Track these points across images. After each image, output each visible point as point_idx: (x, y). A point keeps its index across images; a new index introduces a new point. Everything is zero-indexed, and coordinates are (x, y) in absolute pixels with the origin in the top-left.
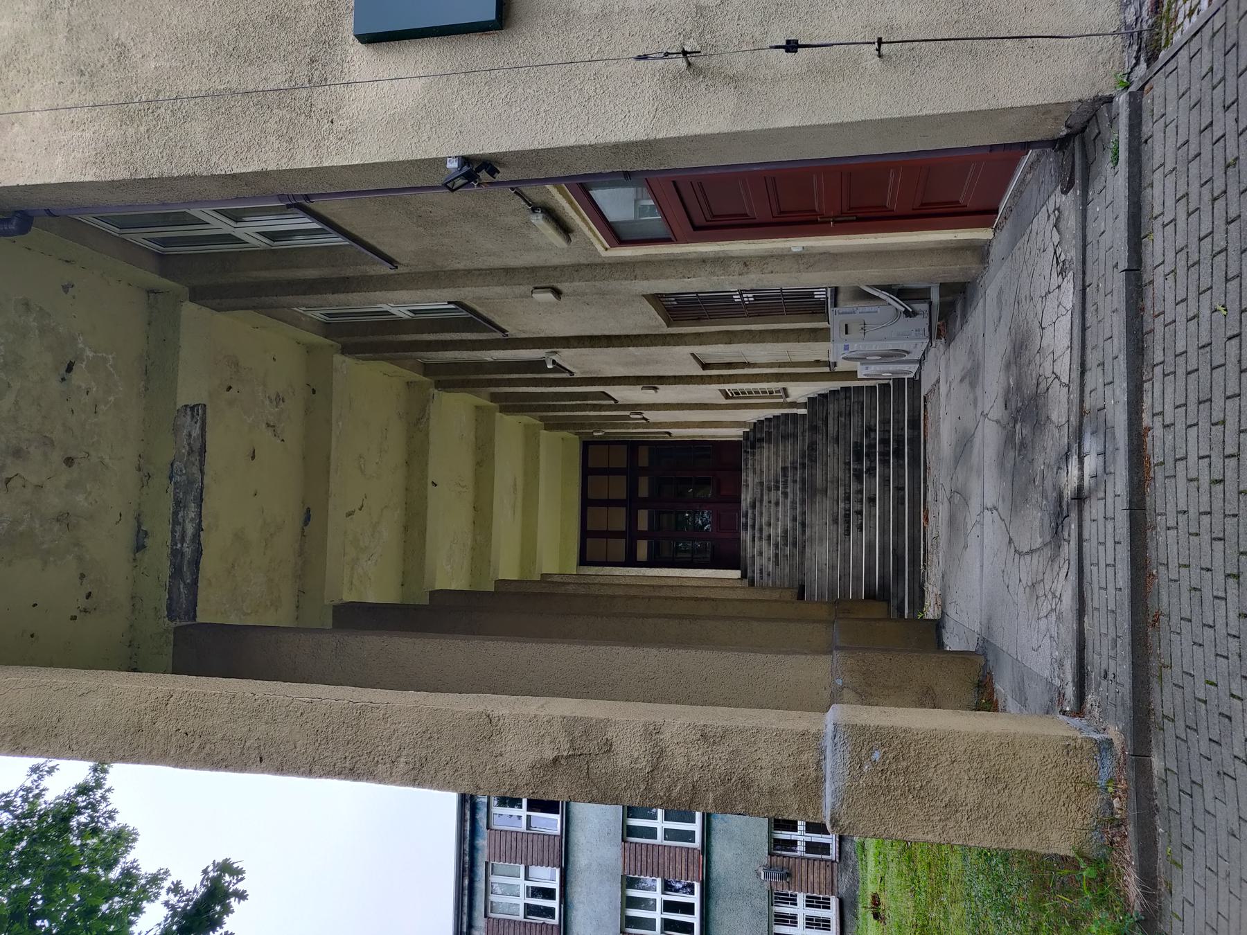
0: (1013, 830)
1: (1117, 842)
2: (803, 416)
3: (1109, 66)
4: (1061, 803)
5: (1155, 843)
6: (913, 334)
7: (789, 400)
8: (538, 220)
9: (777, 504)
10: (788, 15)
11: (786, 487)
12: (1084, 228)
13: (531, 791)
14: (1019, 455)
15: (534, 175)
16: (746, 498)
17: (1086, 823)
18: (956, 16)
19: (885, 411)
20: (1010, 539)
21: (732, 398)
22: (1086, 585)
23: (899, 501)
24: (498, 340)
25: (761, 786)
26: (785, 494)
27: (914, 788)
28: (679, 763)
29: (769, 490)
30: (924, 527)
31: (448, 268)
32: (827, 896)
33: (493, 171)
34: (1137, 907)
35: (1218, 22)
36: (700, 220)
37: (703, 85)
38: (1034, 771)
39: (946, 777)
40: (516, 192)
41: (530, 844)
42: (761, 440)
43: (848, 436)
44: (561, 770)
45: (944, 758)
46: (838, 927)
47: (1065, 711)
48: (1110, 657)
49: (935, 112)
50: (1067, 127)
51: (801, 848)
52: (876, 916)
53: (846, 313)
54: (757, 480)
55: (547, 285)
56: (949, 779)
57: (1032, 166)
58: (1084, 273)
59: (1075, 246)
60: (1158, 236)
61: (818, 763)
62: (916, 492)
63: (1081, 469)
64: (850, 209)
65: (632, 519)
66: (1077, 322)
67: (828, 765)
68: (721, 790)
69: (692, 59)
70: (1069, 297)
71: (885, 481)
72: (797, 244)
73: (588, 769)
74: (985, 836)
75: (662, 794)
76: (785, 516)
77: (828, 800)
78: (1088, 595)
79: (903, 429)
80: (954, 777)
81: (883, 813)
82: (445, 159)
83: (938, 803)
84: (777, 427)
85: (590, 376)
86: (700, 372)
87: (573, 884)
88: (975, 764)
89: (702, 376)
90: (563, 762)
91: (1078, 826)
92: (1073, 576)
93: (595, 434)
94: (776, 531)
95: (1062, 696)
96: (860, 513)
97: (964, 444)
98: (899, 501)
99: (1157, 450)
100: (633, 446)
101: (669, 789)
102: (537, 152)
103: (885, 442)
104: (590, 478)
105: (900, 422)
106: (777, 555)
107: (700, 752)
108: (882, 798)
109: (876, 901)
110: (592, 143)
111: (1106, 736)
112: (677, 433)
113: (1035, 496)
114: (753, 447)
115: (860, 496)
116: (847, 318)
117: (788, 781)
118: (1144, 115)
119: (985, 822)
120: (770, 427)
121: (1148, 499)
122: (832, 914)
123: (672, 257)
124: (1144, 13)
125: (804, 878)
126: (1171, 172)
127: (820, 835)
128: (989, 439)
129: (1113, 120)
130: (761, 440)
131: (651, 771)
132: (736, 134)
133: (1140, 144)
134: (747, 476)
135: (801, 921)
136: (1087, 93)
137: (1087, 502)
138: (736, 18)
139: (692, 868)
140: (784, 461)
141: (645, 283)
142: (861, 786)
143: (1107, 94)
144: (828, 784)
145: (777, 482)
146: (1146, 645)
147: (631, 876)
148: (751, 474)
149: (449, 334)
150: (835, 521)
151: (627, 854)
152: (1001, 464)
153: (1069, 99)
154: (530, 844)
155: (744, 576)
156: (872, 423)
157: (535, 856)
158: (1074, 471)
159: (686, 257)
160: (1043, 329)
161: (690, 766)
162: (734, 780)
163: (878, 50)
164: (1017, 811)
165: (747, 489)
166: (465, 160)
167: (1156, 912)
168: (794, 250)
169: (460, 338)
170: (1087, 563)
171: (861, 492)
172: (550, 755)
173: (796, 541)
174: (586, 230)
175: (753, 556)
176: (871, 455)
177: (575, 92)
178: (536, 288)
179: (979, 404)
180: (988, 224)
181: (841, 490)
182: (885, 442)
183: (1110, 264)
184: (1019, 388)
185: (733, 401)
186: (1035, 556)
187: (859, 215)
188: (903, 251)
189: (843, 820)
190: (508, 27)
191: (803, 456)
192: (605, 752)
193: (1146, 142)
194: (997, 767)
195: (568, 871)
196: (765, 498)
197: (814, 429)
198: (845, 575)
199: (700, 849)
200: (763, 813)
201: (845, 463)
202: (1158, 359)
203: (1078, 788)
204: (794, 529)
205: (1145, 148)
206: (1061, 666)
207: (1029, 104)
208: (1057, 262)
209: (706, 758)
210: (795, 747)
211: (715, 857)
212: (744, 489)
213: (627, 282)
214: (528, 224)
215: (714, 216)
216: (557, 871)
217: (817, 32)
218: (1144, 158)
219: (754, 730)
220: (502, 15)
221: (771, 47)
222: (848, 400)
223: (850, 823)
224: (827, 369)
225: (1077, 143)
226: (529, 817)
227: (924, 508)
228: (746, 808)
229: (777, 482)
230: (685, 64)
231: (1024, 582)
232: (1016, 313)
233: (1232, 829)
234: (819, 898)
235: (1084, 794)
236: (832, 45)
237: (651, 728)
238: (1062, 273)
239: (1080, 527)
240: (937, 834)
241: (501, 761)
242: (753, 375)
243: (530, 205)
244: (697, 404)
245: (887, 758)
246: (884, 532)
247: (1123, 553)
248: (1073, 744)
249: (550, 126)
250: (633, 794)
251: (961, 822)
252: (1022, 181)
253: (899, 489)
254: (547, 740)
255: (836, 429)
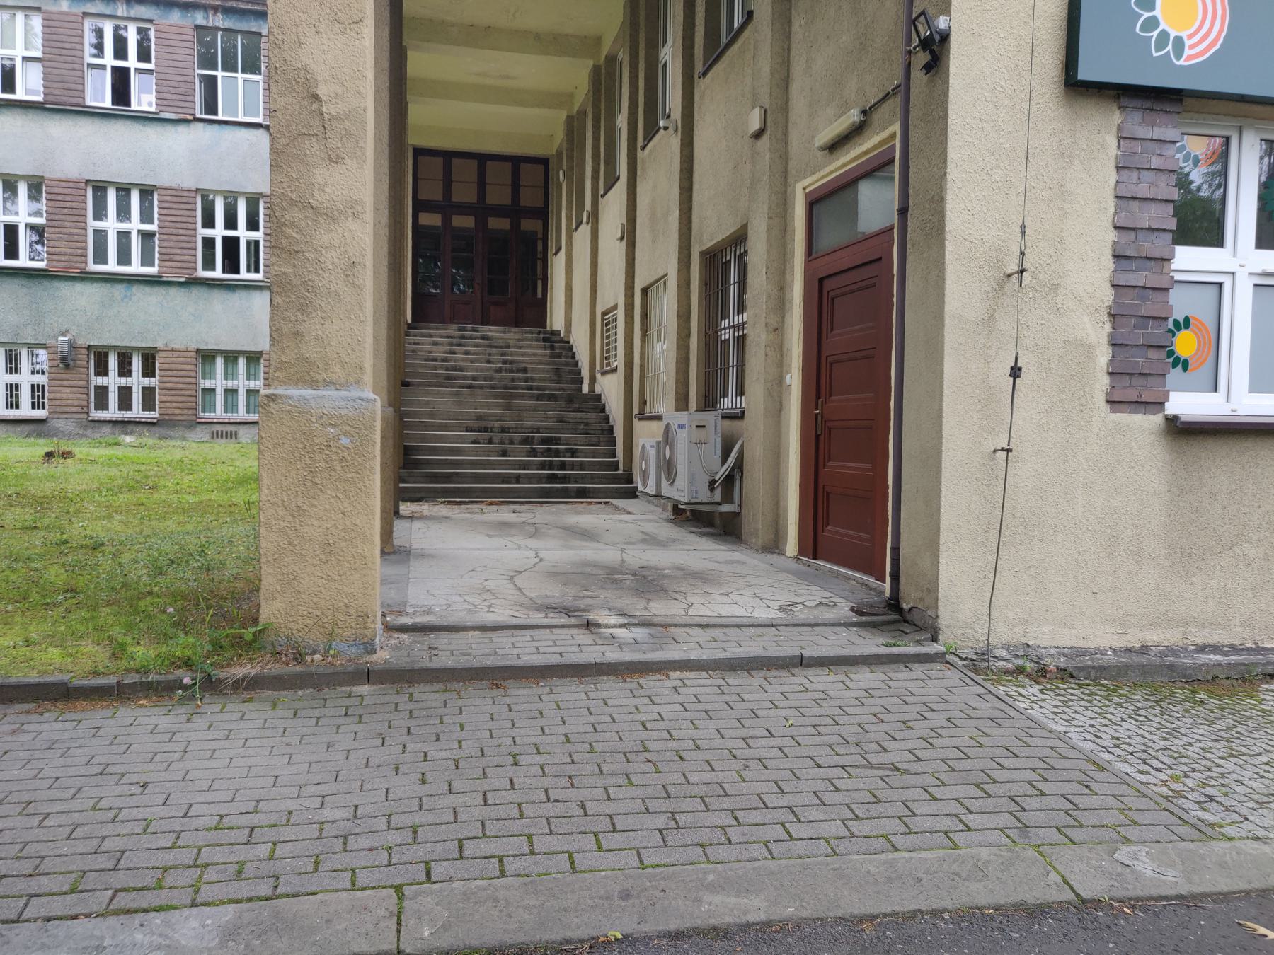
0: (279, 568)
1: (281, 658)
2: (580, 390)
3: (962, 638)
4: (311, 611)
5: (287, 689)
6: (694, 488)
7: (598, 376)
8: (854, 116)
9: (489, 362)
10: (1040, 370)
11: (506, 371)
12: (825, 625)
13: (278, 66)
14: (604, 578)
15: (913, 114)
16: (492, 331)
17: (294, 632)
18: (1019, 515)
19: (592, 466)
20: (520, 572)
21: (603, 319)
22: (509, 632)
23: (505, 479)
24: (693, 67)
25: (304, 324)
26: (499, 370)
27: (313, 477)
28: (323, 237)
29: (502, 355)
30: (483, 502)
31: (793, 12)
32: (47, 406)
33: (928, 68)
34: (222, 675)
35: (1013, 713)
36: (829, 285)
37: (989, 288)
38: (340, 587)
39: (327, 506)
40: (889, 93)
41: (71, 66)
42: (552, 347)
43: (566, 431)
44: (305, 103)
45: (346, 505)
46: (12, 418)
47: (385, 616)
48: (452, 651)
49: (943, 499)
50: (911, 609)
51: (100, 381)
52: (49, 455)
53: (716, 427)
54: (511, 342)
55: (768, 124)
56: (326, 510)
57: (864, 584)
58: (787, 625)
59: (808, 618)
60: (831, 678)
61: (331, 383)
62: (516, 495)
63: (615, 626)
64: (830, 429)
65: (463, 209)
66: (745, 621)
67: (331, 393)
68: (296, 281)
69: (1015, 279)
70: (762, 614)
71: (524, 466)
72: (794, 379)
73: (310, 135)
74: (271, 542)
75: (287, 217)
76: (477, 369)
77: (295, 392)
78: (499, 633)
79: (576, 482)
80: (329, 515)
81: (285, 446)
82: (950, 15)
83: (300, 500)
84: (567, 364)
85: (639, 169)
86: (638, 287)
87: (24, 116)
88: (343, 534)
89: (633, 288)
90: (315, 106)
91: (291, 625)
92: (515, 621)
93: (561, 173)
94: (459, 360)
95: (400, 614)
96: (490, 441)
97: (587, 535)
98: (505, 479)
99: (652, 683)
100: (543, 213)
101: (293, 225)
102: (945, 118)
103: (563, 466)
104: (509, 165)
105: (583, 479)
106: (435, 360)
107: (336, 260)
108: (301, 446)
109: (66, 455)
110: (948, 176)
111: (378, 649)
112: (558, 265)
113: (572, 592)
114: (545, 340)
115: (507, 442)
116: (711, 427)
117: (311, 351)
118: (927, 665)
119: (286, 542)
120: (566, 357)
121: (605, 678)
122: (26, 411)
123: (789, 256)
124: (1001, 663)
125: (65, 383)
126: (887, 685)
127: (140, 401)
128: (608, 555)
129: (918, 643)
130: (552, 347)
131: (312, 207)
132: (942, 318)
133: (904, 662)
134: (515, 333)
135: (13, 378)
136: (943, 621)
137: (587, 632)
138: (1043, 322)
139: (63, 259)
140: (533, 370)
141: (763, 227)
142: (312, 425)
143: (940, 637)
144: (310, 392)
145: (511, 363)
146: (472, 679)
147: (44, 188)
148: (518, 336)
149: (703, 10)
150: (479, 418)
151: (71, 185)
152: (586, 564)
153: (940, 608)
154: (71, 66)
155: (409, 326)
156: (579, 454)
157: (55, 71)
158: (614, 620)
159: (787, 272)
160: (728, 595)
161: (320, 249)
162: (308, 295)
163: (1003, 449)
164: (299, 572)
165: (501, 332)
166: (945, 37)
167: (221, 691)
168: (788, 377)
169: (697, 23)
170: (531, 632)
171: (512, 443)
172: (322, 91)
173: (452, 378)
174: (832, 167)
175: (431, 336)
176: (548, 452)
177: (997, 160)
178: (765, 111)
179: (631, 547)
180: (802, 551)
181: (512, 424)
182: (563, 466)
183: (803, 644)
184: (665, 577)
185: (602, 322)
186: (516, 592)
187: (822, 438)
188: (778, 478)
189: (275, 406)
190: (1066, 93)
191: (538, 388)
192: (329, 155)
193: (907, 667)
194: (341, 554)
195: (39, 111)
196: (494, 350)
197: (570, 399)
198: (426, 426)
199: (87, 270)
200: (275, 325)
201: (539, 429)
202: (731, 682)
203: (326, 625)
204: (465, 378)
205: (902, 666)
206: (428, 613)
207: (940, 576)
208: (790, 605)
209: (330, 267)
210: (347, 360)
211: (79, 287)
212: (501, 328)
213: (766, 210)
214: (845, 107)
215: (833, 299)
216: (40, 98)
217: (1022, 395)
218: (893, 666)
219: (363, 318)
220: (1078, 86)
221: (1017, 353)
222: (600, 432)
223: (272, 413)
224: (636, 410)
225: (895, 617)
226: (103, 67)
227: (502, 502)
228: (279, 307)
229: (511, 363)
230: (1010, 272)
231: (486, 583)
232: (730, 574)
233: (334, 745)
234: (43, 398)
235: (322, 630)
236: (1012, 409)
237: (359, 208)
238: (781, 609)
239: (563, 626)
240: (269, 498)
241: (310, 32)
242: (632, 340)
243: (870, 108)
244: (596, 282)
245: (343, 451)
246: (474, 464)
247: (554, 660)
248: (369, 620)
249: (968, 132)
250: (284, 185)
251: (283, 521)
252: (848, 578)
253: (518, 479)
254: (339, 89)
255: (571, 421)
